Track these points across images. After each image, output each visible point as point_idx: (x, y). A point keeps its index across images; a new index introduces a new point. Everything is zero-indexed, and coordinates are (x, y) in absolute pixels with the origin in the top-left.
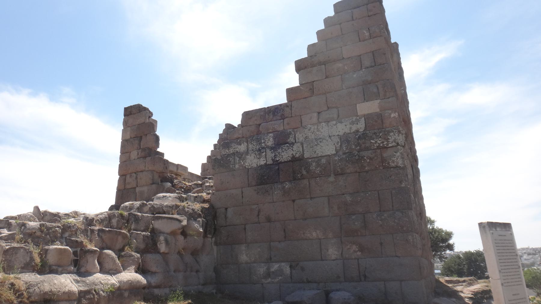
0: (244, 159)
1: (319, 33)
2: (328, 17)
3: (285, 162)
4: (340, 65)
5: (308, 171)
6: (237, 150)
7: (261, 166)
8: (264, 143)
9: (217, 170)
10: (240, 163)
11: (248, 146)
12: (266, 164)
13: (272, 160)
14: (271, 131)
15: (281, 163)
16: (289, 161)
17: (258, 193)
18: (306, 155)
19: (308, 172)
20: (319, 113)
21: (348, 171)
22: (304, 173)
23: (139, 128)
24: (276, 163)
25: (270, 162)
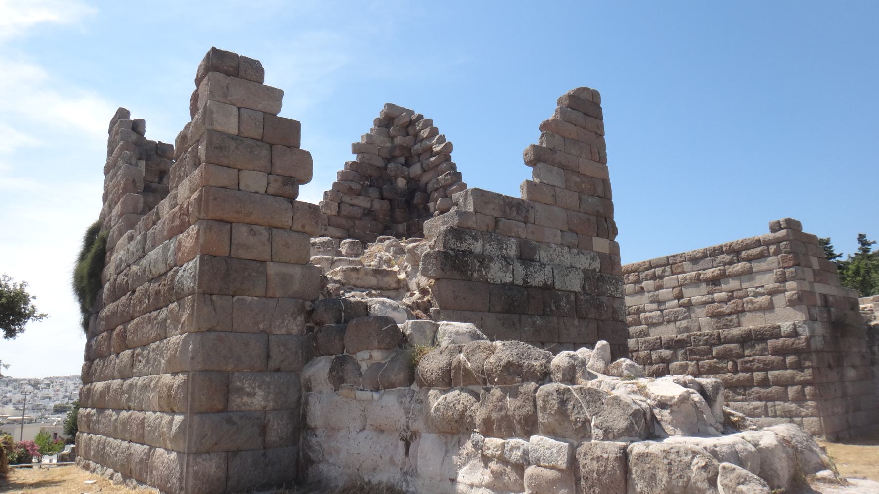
0: (487, 267)
1: (545, 127)
2: (259, 63)
3: (536, 287)
4: (578, 179)
5: (558, 307)
6: (472, 247)
7: (506, 284)
8: (506, 249)
9: (449, 273)
10: (480, 271)
11: (484, 246)
12: (512, 283)
13: (523, 279)
14: (513, 234)
15: (531, 287)
16: (539, 287)
17: (503, 324)
18: (558, 285)
19: (557, 308)
20: (239, 170)
21: (590, 316)
22: (554, 308)
23: (874, 243)
24: (526, 286)
25: (519, 282)
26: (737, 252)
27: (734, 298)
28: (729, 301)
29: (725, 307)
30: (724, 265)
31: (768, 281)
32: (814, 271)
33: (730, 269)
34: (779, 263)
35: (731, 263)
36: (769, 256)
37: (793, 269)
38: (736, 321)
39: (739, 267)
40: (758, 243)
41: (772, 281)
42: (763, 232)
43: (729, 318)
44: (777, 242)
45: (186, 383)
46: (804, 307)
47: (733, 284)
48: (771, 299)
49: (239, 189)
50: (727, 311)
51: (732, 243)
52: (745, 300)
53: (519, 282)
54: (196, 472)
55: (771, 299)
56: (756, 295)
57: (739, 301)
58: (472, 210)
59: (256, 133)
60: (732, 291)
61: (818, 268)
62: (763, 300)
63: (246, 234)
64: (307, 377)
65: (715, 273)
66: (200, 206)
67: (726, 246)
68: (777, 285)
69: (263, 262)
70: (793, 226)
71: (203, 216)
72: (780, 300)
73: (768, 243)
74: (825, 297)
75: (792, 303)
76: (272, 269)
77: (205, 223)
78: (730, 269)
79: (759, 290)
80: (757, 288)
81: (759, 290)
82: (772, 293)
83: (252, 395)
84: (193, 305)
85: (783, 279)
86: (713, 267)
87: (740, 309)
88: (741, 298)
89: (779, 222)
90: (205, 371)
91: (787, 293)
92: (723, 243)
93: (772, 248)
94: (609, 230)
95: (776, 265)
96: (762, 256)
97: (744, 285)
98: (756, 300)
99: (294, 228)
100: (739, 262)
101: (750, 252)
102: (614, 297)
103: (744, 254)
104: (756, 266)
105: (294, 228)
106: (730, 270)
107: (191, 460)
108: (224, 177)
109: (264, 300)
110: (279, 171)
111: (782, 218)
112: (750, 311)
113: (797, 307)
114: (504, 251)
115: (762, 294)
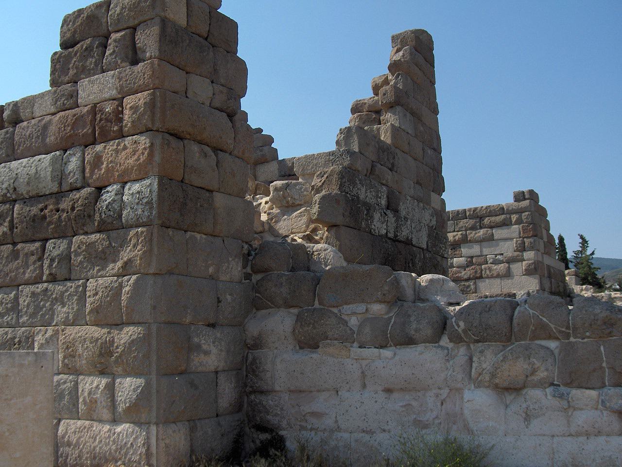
25: (391, 235)
26: (481, 218)
27: (473, 264)
28: (468, 266)
29: (463, 273)
30: (466, 230)
31: (508, 249)
32: (544, 242)
33: (472, 235)
34: (520, 233)
35: (473, 228)
36: (511, 224)
37: (531, 240)
38: (472, 287)
39: (481, 232)
40: (501, 210)
41: (511, 250)
42: (506, 199)
43: (467, 284)
44: (520, 211)
45: (145, 339)
46: (538, 276)
47: (475, 250)
48: (509, 267)
49: (187, 97)
50: (465, 277)
51: (476, 209)
52: (483, 266)
53: (391, 235)
54: (167, 446)
55: (509, 267)
56: (496, 262)
57: (478, 267)
58: (357, 150)
59: (203, 29)
60: (472, 257)
61: (547, 241)
62: (502, 267)
63: (197, 155)
64: (255, 334)
65: (457, 238)
66: (153, 114)
67: (470, 210)
68: (516, 254)
69: (210, 191)
70: (533, 196)
71: (158, 125)
72: (518, 268)
73: (511, 212)
74: (548, 266)
75: (529, 272)
76: (220, 200)
77: (160, 136)
78: (472, 235)
79: (499, 257)
80: (496, 255)
81: (499, 257)
82: (510, 261)
83: (207, 353)
84: (151, 240)
85: (522, 248)
86: (454, 231)
87: (478, 275)
88: (480, 265)
89: (523, 192)
90: (169, 323)
91: (524, 263)
92: (467, 207)
93: (514, 218)
94: (440, 188)
95: (516, 234)
96: (506, 224)
97: (486, 251)
98: (495, 267)
99: (235, 152)
100: (481, 228)
101: (493, 219)
102: (443, 257)
103: (486, 221)
104: (498, 233)
105: (235, 152)
106: (472, 235)
107: (161, 432)
108: (176, 79)
109: (210, 238)
110: (222, 81)
111: (525, 189)
112: (488, 277)
113: (532, 276)
114: (379, 200)
115: (502, 262)
